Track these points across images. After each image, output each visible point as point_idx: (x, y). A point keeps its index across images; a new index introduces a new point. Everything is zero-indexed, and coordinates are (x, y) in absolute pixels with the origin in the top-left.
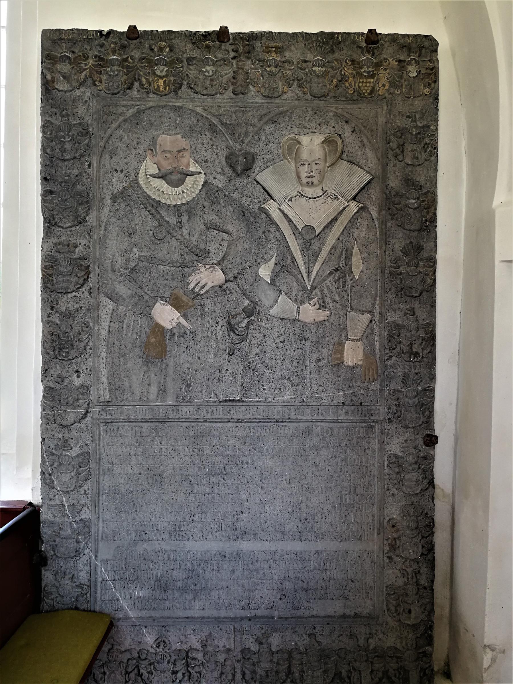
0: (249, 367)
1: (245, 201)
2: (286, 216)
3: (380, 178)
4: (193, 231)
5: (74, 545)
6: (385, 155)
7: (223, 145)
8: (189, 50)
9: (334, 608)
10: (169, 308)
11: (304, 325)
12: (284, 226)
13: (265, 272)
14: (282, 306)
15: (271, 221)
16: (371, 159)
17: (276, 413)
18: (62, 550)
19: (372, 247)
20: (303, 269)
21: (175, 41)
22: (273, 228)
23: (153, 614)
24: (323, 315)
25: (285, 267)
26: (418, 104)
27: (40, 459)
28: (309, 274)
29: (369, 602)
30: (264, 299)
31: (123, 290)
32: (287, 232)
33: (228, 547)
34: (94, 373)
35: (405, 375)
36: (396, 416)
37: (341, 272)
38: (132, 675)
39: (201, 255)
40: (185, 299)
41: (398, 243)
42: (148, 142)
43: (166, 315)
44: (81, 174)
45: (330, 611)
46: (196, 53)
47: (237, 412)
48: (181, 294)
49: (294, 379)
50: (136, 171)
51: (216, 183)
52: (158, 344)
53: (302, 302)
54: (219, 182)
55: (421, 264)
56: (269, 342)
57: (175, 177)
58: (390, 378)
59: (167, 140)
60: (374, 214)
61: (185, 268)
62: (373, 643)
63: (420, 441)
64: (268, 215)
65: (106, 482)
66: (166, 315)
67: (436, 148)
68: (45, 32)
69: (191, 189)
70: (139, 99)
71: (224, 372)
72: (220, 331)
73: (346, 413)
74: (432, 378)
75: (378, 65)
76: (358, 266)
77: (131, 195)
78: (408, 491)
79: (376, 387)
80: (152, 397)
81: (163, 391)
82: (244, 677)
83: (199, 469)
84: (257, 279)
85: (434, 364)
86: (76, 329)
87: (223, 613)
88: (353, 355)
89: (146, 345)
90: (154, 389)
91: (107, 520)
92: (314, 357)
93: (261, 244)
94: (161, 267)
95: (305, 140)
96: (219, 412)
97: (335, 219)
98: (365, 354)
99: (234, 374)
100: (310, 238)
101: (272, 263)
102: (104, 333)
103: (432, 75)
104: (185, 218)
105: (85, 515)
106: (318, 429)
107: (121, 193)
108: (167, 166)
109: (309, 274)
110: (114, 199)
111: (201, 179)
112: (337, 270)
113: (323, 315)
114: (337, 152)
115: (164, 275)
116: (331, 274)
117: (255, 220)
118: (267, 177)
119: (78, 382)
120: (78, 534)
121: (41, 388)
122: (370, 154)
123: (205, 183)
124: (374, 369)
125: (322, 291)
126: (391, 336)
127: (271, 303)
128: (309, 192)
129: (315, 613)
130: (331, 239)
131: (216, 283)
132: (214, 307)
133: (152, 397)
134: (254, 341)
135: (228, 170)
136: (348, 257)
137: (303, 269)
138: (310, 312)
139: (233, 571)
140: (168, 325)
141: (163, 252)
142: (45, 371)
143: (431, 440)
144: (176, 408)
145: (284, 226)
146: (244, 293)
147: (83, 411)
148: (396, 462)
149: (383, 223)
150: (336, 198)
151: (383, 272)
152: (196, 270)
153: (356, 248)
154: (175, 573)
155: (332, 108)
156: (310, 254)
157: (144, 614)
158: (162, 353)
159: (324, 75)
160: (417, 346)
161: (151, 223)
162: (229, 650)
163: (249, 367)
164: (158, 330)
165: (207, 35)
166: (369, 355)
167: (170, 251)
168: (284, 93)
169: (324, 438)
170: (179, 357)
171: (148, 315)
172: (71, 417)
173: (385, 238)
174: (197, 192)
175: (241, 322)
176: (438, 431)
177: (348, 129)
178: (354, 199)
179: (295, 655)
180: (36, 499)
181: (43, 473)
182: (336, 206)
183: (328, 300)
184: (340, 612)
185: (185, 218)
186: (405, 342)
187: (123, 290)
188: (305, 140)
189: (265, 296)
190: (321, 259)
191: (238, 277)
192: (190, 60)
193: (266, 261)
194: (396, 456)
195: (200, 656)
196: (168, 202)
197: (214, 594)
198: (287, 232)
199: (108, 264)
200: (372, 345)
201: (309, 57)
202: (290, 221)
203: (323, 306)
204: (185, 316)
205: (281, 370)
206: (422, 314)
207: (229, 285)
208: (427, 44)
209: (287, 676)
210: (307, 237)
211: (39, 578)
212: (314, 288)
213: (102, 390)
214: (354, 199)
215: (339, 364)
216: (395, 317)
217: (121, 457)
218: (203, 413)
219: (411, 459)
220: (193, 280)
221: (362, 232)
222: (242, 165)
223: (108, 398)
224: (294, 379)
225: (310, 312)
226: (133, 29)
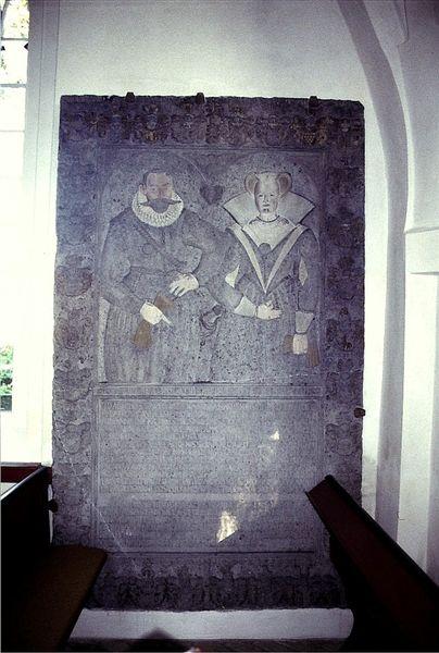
0: (216, 355)
1: (216, 224)
2: (247, 235)
3: (321, 207)
4: (175, 247)
5: (78, 495)
6: (324, 191)
7: (198, 181)
8: (173, 110)
9: (285, 545)
10: (154, 309)
11: (261, 321)
12: (245, 243)
13: (231, 279)
14: (244, 306)
15: (236, 240)
16: (313, 191)
17: (239, 391)
18: (69, 499)
19: (315, 261)
20: (260, 277)
21: (163, 104)
22: (237, 246)
23: (140, 550)
24: (277, 313)
25: (247, 276)
26: (349, 151)
27: (52, 428)
28: (265, 281)
29: (309, 540)
30: (229, 301)
31: (119, 294)
32: (249, 249)
33: (199, 498)
34: (93, 358)
35: (340, 361)
36: (332, 394)
37: (291, 280)
38: (123, 597)
39: (178, 267)
40: (166, 300)
41: (335, 258)
42: (140, 179)
43: (152, 314)
44: (87, 203)
45: (279, 547)
46: (179, 112)
47: (207, 390)
48: (163, 296)
49: (253, 365)
50: (130, 200)
51: (193, 209)
52: (144, 337)
53: (260, 303)
54: (195, 208)
55: (353, 274)
56: (233, 335)
57: (160, 205)
58: (328, 364)
59: (155, 178)
60: (316, 234)
61: (167, 276)
62: (312, 572)
63: (351, 414)
64: (233, 235)
65: (102, 447)
66: (152, 314)
67: (363, 185)
68: (65, 99)
69: (172, 216)
70: (135, 147)
71: (196, 359)
72: (194, 326)
73: (294, 392)
74: (362, 363)
75: (319, 122)
76: (304, 275)
77: (125, 218)
78: (342, 453)
79: (317, 370)
80: (140, 379)
81: (148, 374)
82: (211, 599)
83: (177, 436)
84: (224, 284)
85: (363, 353)
86: (81, 324)
87: (194, 549)
88: (299, 345)
89: (135, 338)
90: (141, 372)
91: (103, 478)
92: (269, 347)
93: (228, 257)
94: (148, 276)
95: (262, 177)
96: (193, 390)
97: (286, 239)
98: (309, 344)
99: (205, 361)
100: (266, 253)
101: (236, 273)
102: (102, 327)
103: (359, 131)
104: (167, 237)
105: (87, 471)
106: (270, 404)
107: (117, 217)
108: (154, 196)
109: (265, 281)
110: (112, 221)
111: (181, 207)
112: (287, 278)
113: (277, 313)
114: (286, 185)
115: (151, 282)
116: (282, 281)
117: (224, 237)
118: (233, 206)
119: (82, 367)
120: (81, 486)
121: (53, 371)
122: (312, 188)
123: (184, 209)
124: (317, 356)
125: (275, 295)
126: (329, 331)
127: (235, 304)
128: (266, 216)
129: (267, 549)
130: (283, 254)
131: (192, 288)
132: (192, 308)
133: (140, 379)
134: (221, 335)
135: (202, 200)
136: (296, 268)
137: (260, 277)
138: (266, 312)
139: (203, 517)
140: (153, 321)
141: (149, 263)
142: (56, 358)
143: (361, 413)
144: (158, 388)
145: (245, 243)
146: (213, 295)
147: (86, 390)
148: (332, 430)
149: (323, 241)
150: (287, 222)
151: (323, 279)
152: (175, 278)
153: (302, 262)
154: (157, 519)
155: (282, 156)
156: (267, 267)
157: (131, 549)
158: (148, 343)
159: (277, 128)
160: (345, 338)
161: (141, 241)
162: (199, 578)
163: (216, 355)
164: (144, 324)
165: (187, 99)
166: (312, 345)
167: (155, 262)
168: (245, 142)
169: (276, 411)
170: (162, 347)
171: (136, 312)
172: (76, 394)
173: (325, 254)
174: (177, 216)
175: (212, 316)
176: (366, 406)
177: (296, 169)
178: (301, 223)
179: (252, 582)
180: (46, 459)
181: (54, 438)
182: (287, 228)
183: (280, 302)
184: (288, 548)
185: (167, 237)
186: (341, 335)
187: (119, 294)
188: (262, 177)
189: (230, 299)
190: (275, 270)
191: (213, 285)
192: (174, 116)
193: (232, 270)
194: (333, 425)
195: (177, 582)
196: (154, 225)
197: (188, 534)
198: (249, 249)
199: (106, 273)
200: (314, 337)
201: (266, 115)
202: (251, 240)
203: (276, 307)
204: (166, 315)
205: (242, 358)
206: (353, 313)
207: (202, 289)
208: (356, 107)
209: (245, 598)
210: (263, 252)
211: (364, 515)
212: (269, 292)
213: (100, 375)
214: (301, 223)
215: (289, 353)
216: (334, 316)
217: (114, 425)
218: (180, 392)
219: (344, 428)
220: (174, 285)
221: (307, 249)
222: (212, 195)
223: (105, 380)
224: (253, 365)
225: (266, 312)
226: (130, 95)
